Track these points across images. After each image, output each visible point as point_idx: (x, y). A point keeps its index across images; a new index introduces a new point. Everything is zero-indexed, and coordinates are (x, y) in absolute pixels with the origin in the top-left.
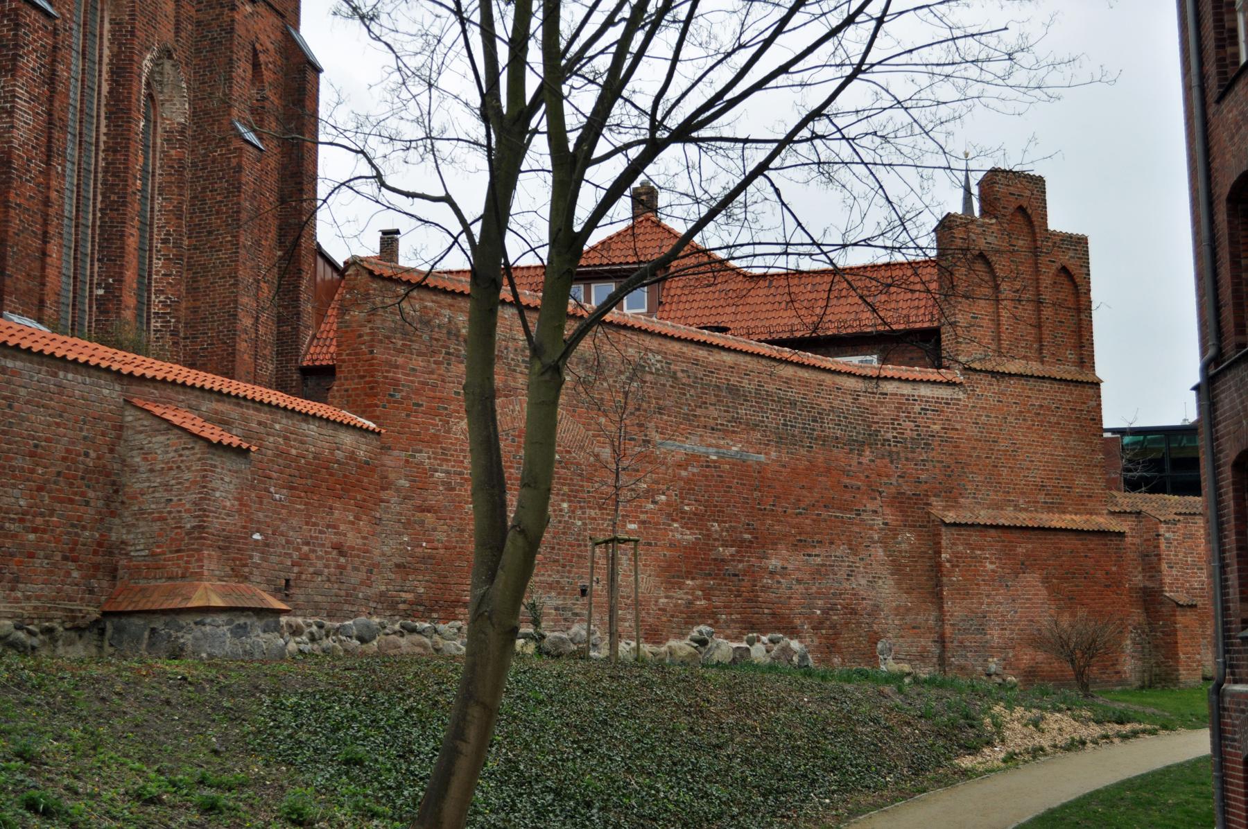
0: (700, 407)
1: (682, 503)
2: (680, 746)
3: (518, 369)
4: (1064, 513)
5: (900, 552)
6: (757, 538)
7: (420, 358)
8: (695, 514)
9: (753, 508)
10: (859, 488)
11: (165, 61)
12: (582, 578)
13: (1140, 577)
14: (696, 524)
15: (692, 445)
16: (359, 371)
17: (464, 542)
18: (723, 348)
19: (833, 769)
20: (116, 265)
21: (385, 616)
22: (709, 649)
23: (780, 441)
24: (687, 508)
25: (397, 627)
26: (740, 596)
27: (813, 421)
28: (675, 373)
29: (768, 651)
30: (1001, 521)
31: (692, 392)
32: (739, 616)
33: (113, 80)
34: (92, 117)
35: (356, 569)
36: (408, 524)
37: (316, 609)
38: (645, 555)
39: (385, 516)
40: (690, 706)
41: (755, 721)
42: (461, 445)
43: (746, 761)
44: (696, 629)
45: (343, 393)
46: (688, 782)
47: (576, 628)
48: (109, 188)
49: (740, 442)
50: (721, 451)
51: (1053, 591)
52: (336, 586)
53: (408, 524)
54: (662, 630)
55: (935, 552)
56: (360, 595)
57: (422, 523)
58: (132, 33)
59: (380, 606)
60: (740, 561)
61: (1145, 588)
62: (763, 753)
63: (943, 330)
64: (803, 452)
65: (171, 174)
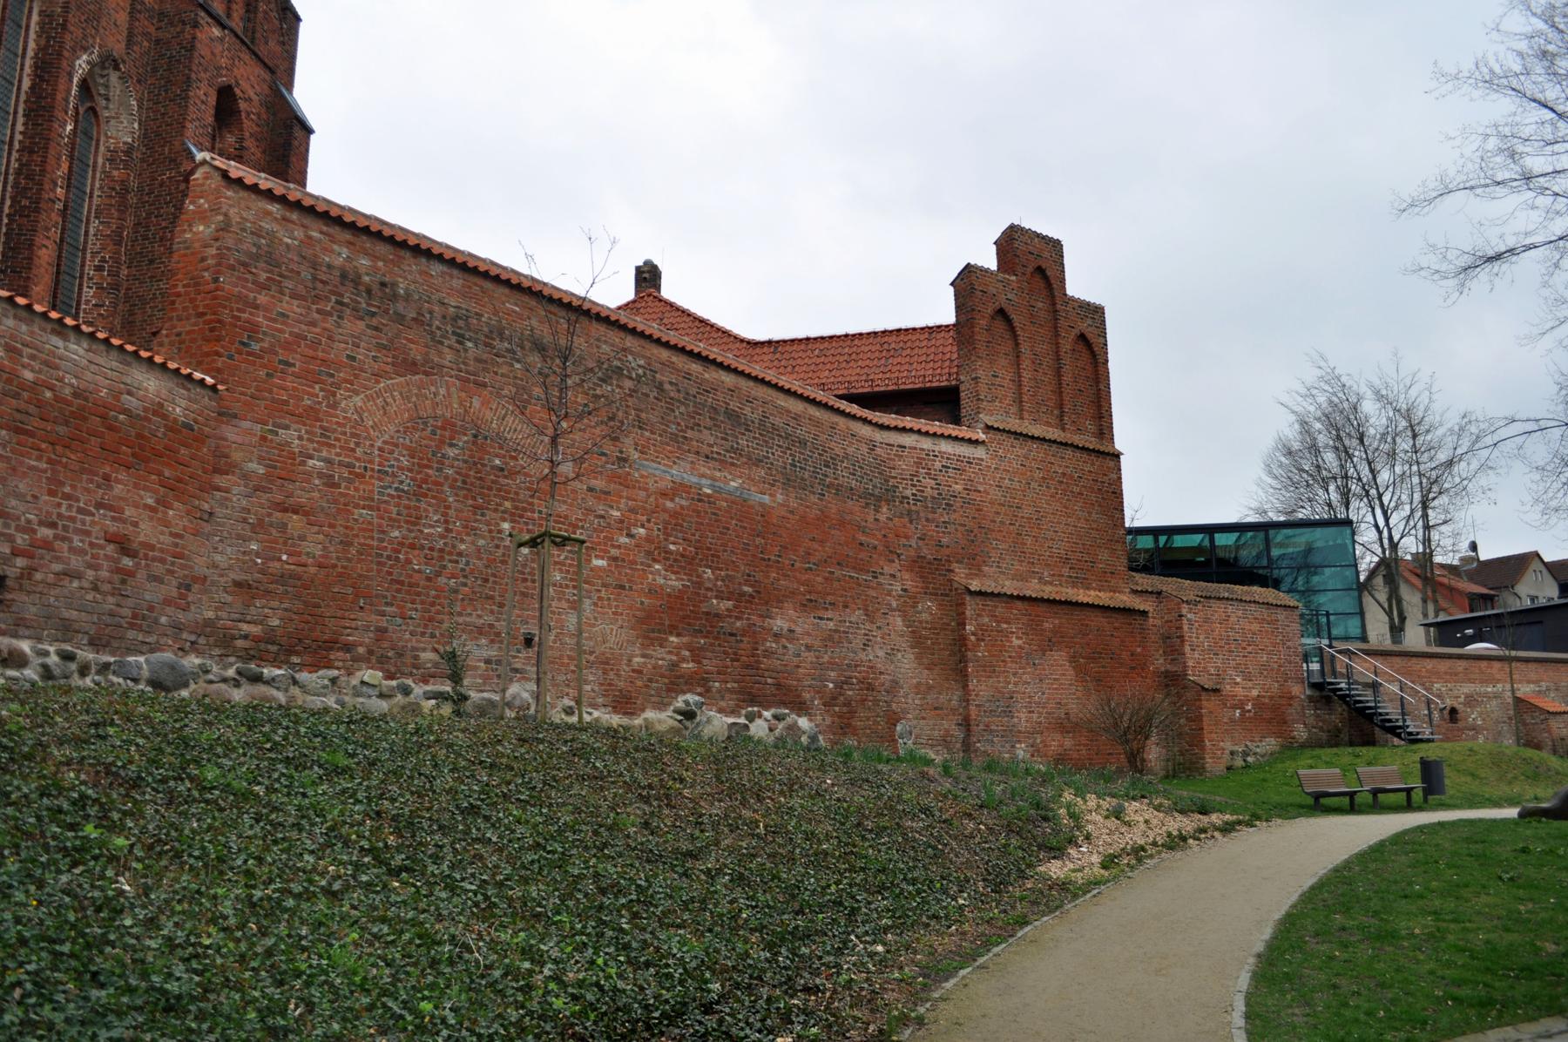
0: (692, 429)
1: (666, 540)
2: (620, 855)
3: (446, 342)
4: (1088, 589)
5: (921, 622)
6: (759, 592)
7: (296, 302)
8: (683, 556)
9: (753, 556)
10: (875, 548)
11: (111, 71)
12: (527, 623)
13: (1161, 661)
14: (685, 568)
15: (680, 472)
16: (197, 306)
17: (349, 560)
18: (721, 365)
19: (882, 888)
20: (20, 277)
21: (212, 657)
22: (698, 724)
23: (788, 483)
24: (672, 547)
25: (231, 672)
26: (738, 660)
27: (825, 466)
28: (661, 384)
29: (771, 730)
30: (1028, 593)
31: (682, 409)
32: (736, 685)
33: (36, 75)
34: (8, 113)
35: (157, 579)
36: (259, 526)
37: (66, 630)
38: (615, 600)
39: (219, 511)
40: (650, 786)
41: (755, 811)
42: (352, 427)
43: (739, 879)
44: (681, 698)
45: (173, 338)
46: (622, 930)
47: (514, 689)
48: (19, 192)
49: (741, 477)
50: (717, 484)
51: (1081, 671)
52: (111, 599)
53: (259, 526)
54: (637, 698)
55: (959, 624)
56: (163, 620)
57: (283, 527)
58: (64, 26)
59: (202, 640)
60: (738, 618)
61: (1167, 671)
62: (768, 865)
63: (962, 388)
64: (814, 499)
65: (111, 196)
